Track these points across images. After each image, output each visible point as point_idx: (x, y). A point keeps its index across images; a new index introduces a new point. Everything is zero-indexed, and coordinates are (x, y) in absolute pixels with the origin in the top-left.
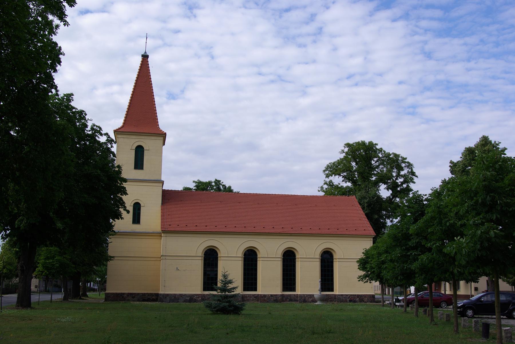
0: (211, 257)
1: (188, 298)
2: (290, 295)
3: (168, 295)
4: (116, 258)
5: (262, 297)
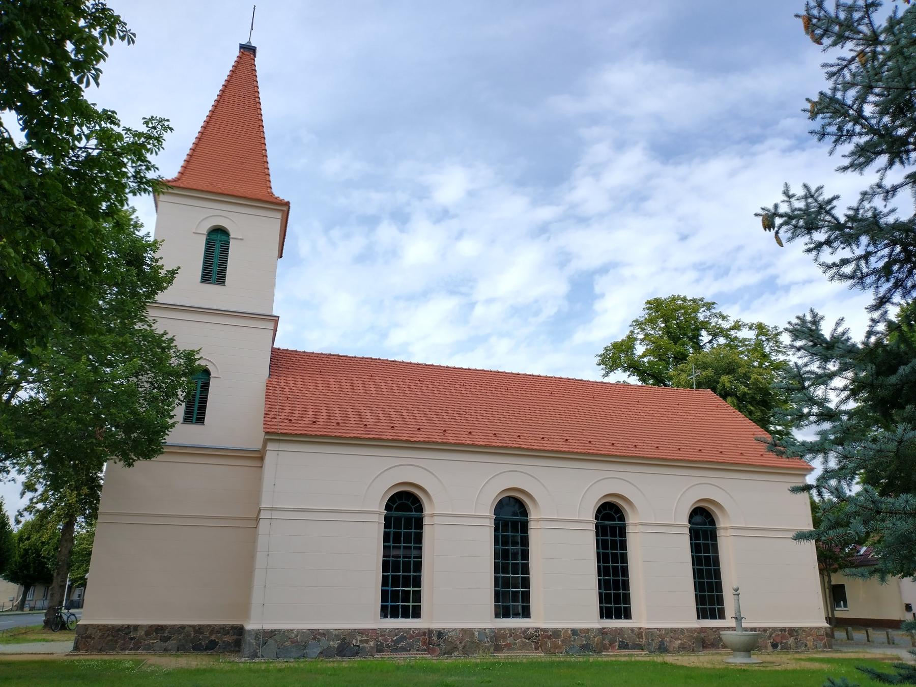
0: (404, 515)
1: (335, 644)
2: (620, 631)
3: (272, 633)
4: (791, 535)
5: (549, 637)
